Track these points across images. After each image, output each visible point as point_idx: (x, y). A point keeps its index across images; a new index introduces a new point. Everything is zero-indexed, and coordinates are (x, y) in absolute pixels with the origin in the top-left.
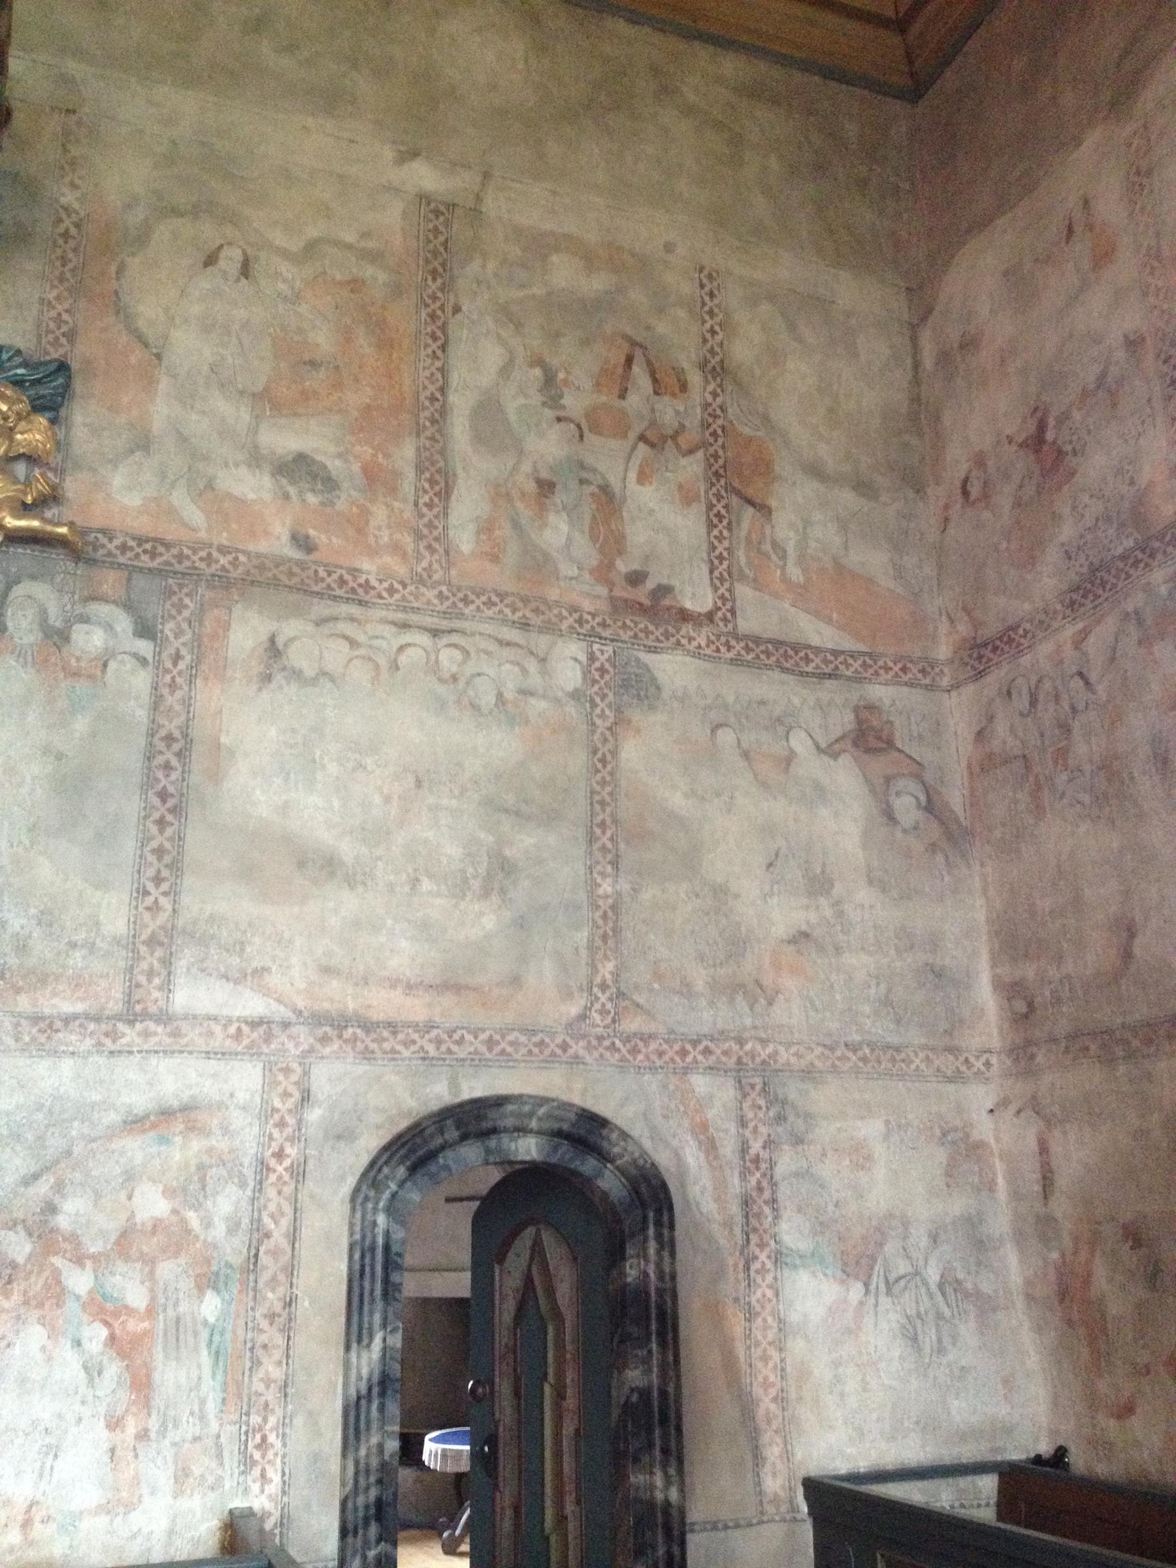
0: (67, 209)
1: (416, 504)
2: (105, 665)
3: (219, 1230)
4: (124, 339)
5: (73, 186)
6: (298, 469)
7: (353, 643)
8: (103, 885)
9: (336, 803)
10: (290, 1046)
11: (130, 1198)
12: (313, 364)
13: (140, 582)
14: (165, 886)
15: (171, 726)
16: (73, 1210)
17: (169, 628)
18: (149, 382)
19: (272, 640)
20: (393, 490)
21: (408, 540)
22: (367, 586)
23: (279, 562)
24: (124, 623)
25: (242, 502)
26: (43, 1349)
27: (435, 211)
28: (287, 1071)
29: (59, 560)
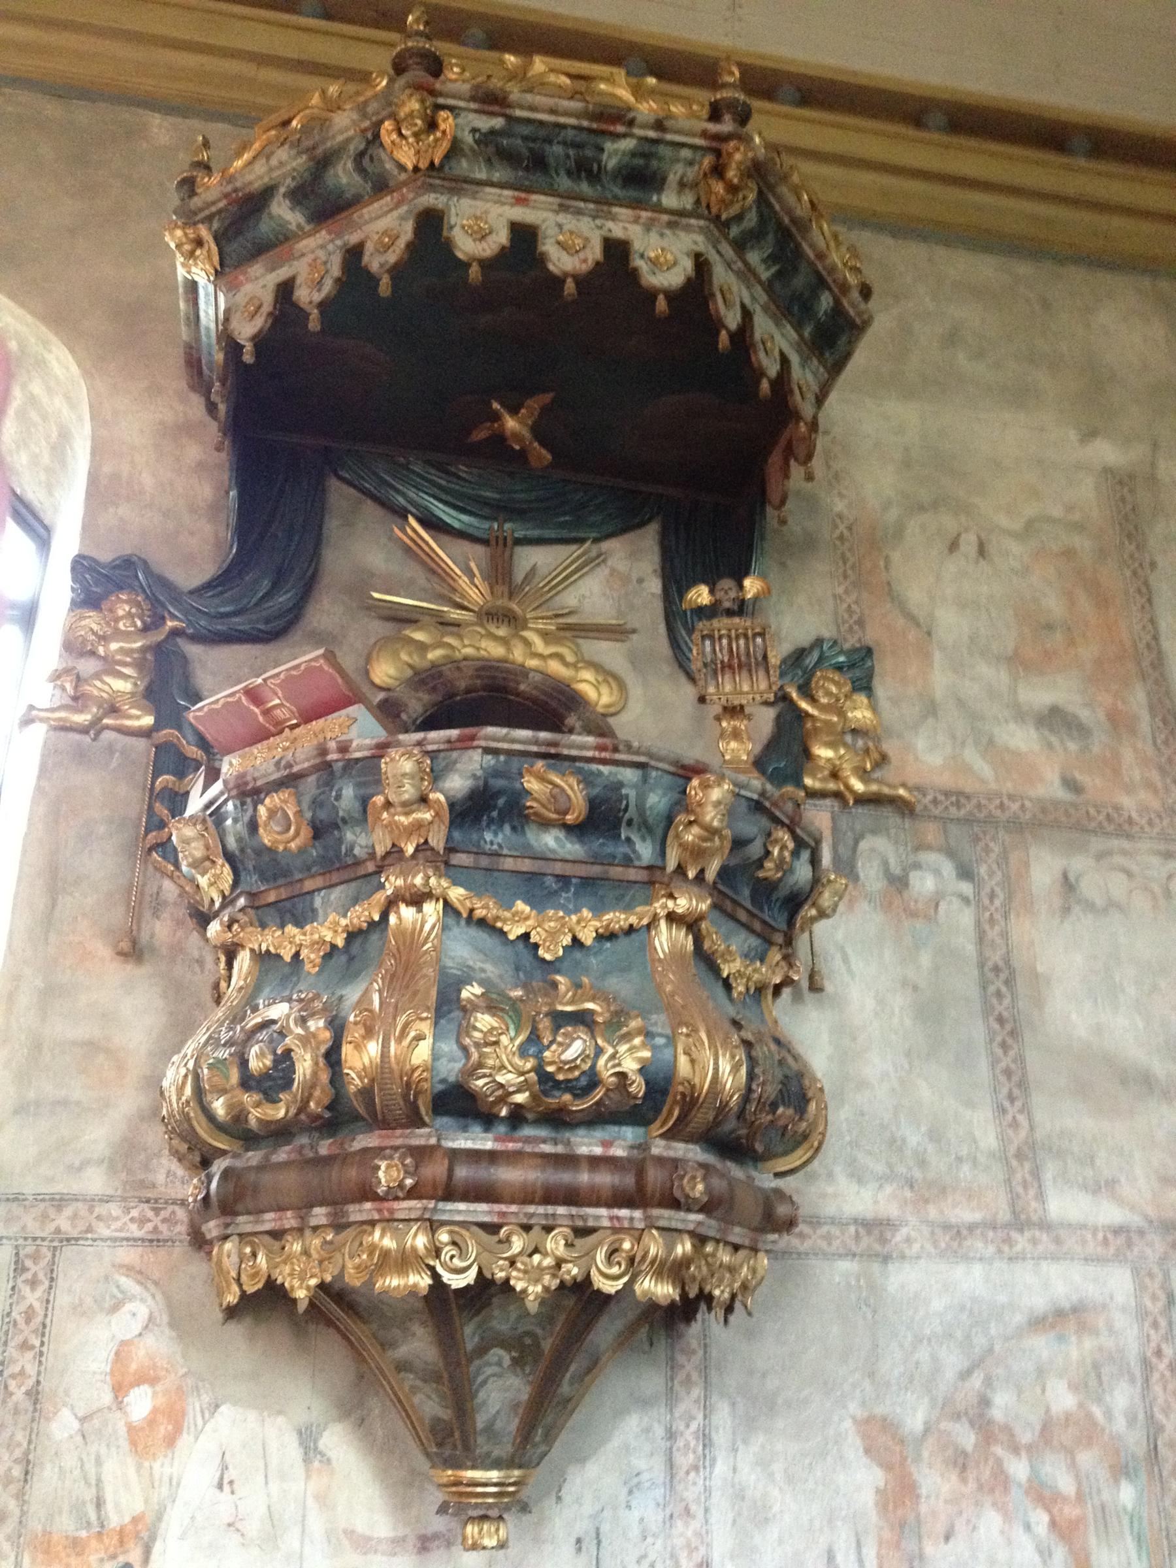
0: (840, 516)
1: (1155, 743)
2: (937, 905)
3: (1120, 1424)
4: (901, 622)
5: (841, 495)
6: (1053, 720)
7: (1129, 874)
8: (970, 1104)
9: (1141, 1025)
10: (1149, 1252)
11: (1044, 1391)
12: (1049, 627)
13: (954, 829)
14: (1018, 1104)
15: (996, 957)
16: (1002, 1402)
17: (983, 870)
18: (926, 657)
19: (1065, 876)
20: (1133, 731)
21: (1155, 776)
22: (1130, 821)
23: (1056, 803)
24: (948, 869)
25: (1017, 754)
26: (1002, 1532)
27: (1120, 483)
28: (1150, 1275)
29: (890, 817)
